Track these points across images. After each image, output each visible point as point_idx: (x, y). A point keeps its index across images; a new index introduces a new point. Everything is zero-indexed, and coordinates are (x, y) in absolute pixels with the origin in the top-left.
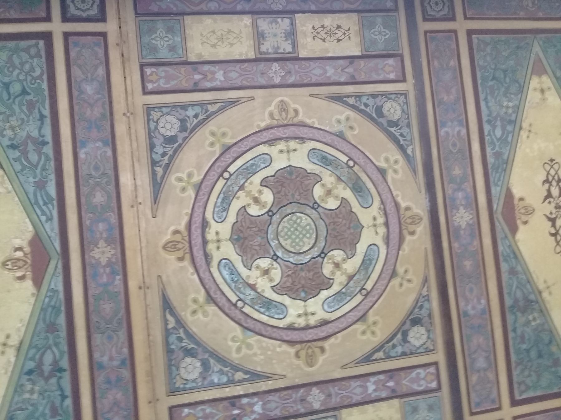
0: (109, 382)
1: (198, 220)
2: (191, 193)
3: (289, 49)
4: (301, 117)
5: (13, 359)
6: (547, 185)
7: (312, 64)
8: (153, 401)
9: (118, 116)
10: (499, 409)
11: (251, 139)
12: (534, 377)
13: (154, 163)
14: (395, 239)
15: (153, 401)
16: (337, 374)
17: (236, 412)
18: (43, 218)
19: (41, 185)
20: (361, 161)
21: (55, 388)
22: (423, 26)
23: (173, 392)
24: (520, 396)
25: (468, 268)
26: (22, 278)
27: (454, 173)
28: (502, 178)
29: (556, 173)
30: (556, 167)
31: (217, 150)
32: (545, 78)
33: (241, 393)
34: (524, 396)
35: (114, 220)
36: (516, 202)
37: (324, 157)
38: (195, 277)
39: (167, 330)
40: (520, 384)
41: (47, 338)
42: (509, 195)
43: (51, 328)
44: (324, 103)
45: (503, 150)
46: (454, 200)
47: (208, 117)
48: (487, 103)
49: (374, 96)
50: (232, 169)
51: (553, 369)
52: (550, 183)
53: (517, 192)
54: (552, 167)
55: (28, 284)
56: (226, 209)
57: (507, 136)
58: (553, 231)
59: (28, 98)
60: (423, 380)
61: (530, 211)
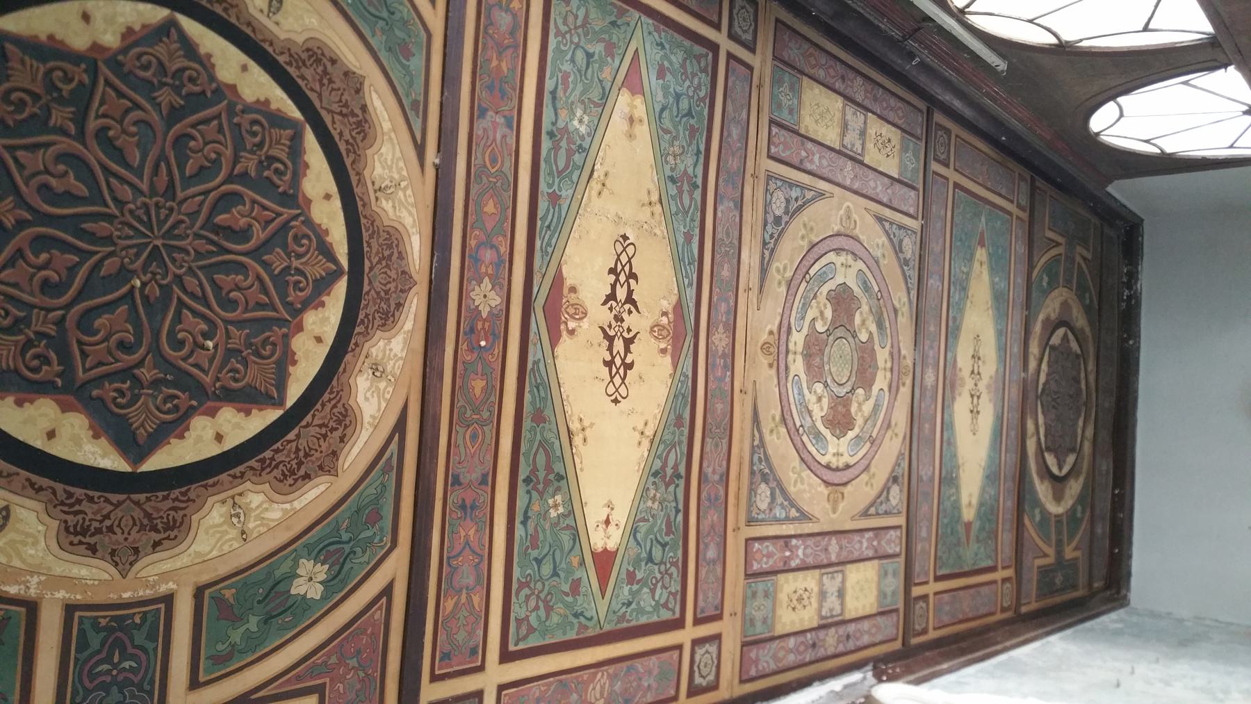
0: (463, 507)
1: (785, 323)
2: (783, 289)
3: (860, 151)
4: (857, 232)
5: (646, 454)
6: (613, 277)
7: (871, 174)
8: (737, 529)
9: (748, 176)
10: (481, 668)
11: (827, 242)
12: (542, 612)
13: (765, 244)
14: (893, 388)
15: (737, 529)
16: (849, 526)
17: (788, 554)
18: (686, 281)
19: (688, 238)
20: (885, 295)
21: (671, 498)
22: (935, 166)
23: (750, 521)
24: (516, 645)
25: (478, 391)
26: (664, 351)
27: (486, 209)
28: (554, 241)
29: (629, 261)
30: (630, 250)
31: (805, 245)
32: (638, 101)
33: (793, 533)
34: (522, 646)
35: (732, 303)
36: (565, 291)
37: (865, 282)
38: (777, 390)
39: (753, 447)
40: (519, 622)
41: (674, 433)
42: (558, 279)
43: (679, 422)
44: (870, 220)
45: (564, 193)
46: (477, 261)
47: (804, 204)
48: (554, 98)
49: (901, 227)
50: (812, 272)
51: (570, 599)
52: (617, 275)
53: (571, 275)
54: (624, 249)
55: (668, 359)
56: (803, 318)
57: (572, 173)
58: (608, 358)
59: (692, 122)
60: (894, 548)
61: (656, 328)
